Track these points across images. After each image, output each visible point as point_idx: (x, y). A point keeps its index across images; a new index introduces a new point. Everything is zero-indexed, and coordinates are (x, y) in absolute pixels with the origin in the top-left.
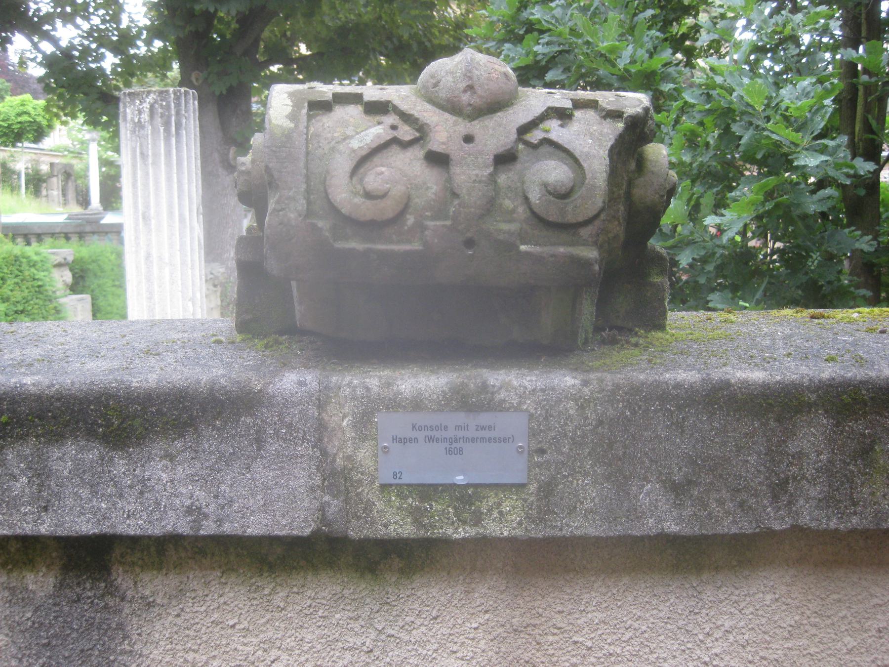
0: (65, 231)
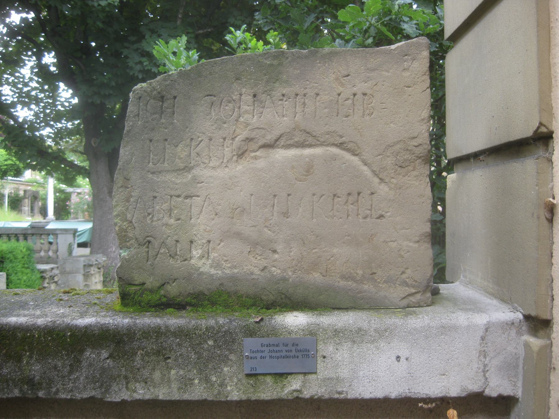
0: (16, 233)
